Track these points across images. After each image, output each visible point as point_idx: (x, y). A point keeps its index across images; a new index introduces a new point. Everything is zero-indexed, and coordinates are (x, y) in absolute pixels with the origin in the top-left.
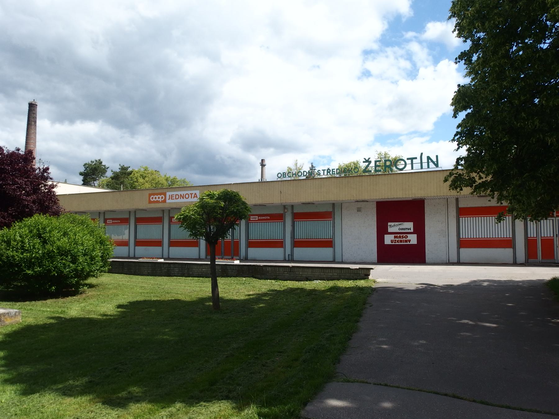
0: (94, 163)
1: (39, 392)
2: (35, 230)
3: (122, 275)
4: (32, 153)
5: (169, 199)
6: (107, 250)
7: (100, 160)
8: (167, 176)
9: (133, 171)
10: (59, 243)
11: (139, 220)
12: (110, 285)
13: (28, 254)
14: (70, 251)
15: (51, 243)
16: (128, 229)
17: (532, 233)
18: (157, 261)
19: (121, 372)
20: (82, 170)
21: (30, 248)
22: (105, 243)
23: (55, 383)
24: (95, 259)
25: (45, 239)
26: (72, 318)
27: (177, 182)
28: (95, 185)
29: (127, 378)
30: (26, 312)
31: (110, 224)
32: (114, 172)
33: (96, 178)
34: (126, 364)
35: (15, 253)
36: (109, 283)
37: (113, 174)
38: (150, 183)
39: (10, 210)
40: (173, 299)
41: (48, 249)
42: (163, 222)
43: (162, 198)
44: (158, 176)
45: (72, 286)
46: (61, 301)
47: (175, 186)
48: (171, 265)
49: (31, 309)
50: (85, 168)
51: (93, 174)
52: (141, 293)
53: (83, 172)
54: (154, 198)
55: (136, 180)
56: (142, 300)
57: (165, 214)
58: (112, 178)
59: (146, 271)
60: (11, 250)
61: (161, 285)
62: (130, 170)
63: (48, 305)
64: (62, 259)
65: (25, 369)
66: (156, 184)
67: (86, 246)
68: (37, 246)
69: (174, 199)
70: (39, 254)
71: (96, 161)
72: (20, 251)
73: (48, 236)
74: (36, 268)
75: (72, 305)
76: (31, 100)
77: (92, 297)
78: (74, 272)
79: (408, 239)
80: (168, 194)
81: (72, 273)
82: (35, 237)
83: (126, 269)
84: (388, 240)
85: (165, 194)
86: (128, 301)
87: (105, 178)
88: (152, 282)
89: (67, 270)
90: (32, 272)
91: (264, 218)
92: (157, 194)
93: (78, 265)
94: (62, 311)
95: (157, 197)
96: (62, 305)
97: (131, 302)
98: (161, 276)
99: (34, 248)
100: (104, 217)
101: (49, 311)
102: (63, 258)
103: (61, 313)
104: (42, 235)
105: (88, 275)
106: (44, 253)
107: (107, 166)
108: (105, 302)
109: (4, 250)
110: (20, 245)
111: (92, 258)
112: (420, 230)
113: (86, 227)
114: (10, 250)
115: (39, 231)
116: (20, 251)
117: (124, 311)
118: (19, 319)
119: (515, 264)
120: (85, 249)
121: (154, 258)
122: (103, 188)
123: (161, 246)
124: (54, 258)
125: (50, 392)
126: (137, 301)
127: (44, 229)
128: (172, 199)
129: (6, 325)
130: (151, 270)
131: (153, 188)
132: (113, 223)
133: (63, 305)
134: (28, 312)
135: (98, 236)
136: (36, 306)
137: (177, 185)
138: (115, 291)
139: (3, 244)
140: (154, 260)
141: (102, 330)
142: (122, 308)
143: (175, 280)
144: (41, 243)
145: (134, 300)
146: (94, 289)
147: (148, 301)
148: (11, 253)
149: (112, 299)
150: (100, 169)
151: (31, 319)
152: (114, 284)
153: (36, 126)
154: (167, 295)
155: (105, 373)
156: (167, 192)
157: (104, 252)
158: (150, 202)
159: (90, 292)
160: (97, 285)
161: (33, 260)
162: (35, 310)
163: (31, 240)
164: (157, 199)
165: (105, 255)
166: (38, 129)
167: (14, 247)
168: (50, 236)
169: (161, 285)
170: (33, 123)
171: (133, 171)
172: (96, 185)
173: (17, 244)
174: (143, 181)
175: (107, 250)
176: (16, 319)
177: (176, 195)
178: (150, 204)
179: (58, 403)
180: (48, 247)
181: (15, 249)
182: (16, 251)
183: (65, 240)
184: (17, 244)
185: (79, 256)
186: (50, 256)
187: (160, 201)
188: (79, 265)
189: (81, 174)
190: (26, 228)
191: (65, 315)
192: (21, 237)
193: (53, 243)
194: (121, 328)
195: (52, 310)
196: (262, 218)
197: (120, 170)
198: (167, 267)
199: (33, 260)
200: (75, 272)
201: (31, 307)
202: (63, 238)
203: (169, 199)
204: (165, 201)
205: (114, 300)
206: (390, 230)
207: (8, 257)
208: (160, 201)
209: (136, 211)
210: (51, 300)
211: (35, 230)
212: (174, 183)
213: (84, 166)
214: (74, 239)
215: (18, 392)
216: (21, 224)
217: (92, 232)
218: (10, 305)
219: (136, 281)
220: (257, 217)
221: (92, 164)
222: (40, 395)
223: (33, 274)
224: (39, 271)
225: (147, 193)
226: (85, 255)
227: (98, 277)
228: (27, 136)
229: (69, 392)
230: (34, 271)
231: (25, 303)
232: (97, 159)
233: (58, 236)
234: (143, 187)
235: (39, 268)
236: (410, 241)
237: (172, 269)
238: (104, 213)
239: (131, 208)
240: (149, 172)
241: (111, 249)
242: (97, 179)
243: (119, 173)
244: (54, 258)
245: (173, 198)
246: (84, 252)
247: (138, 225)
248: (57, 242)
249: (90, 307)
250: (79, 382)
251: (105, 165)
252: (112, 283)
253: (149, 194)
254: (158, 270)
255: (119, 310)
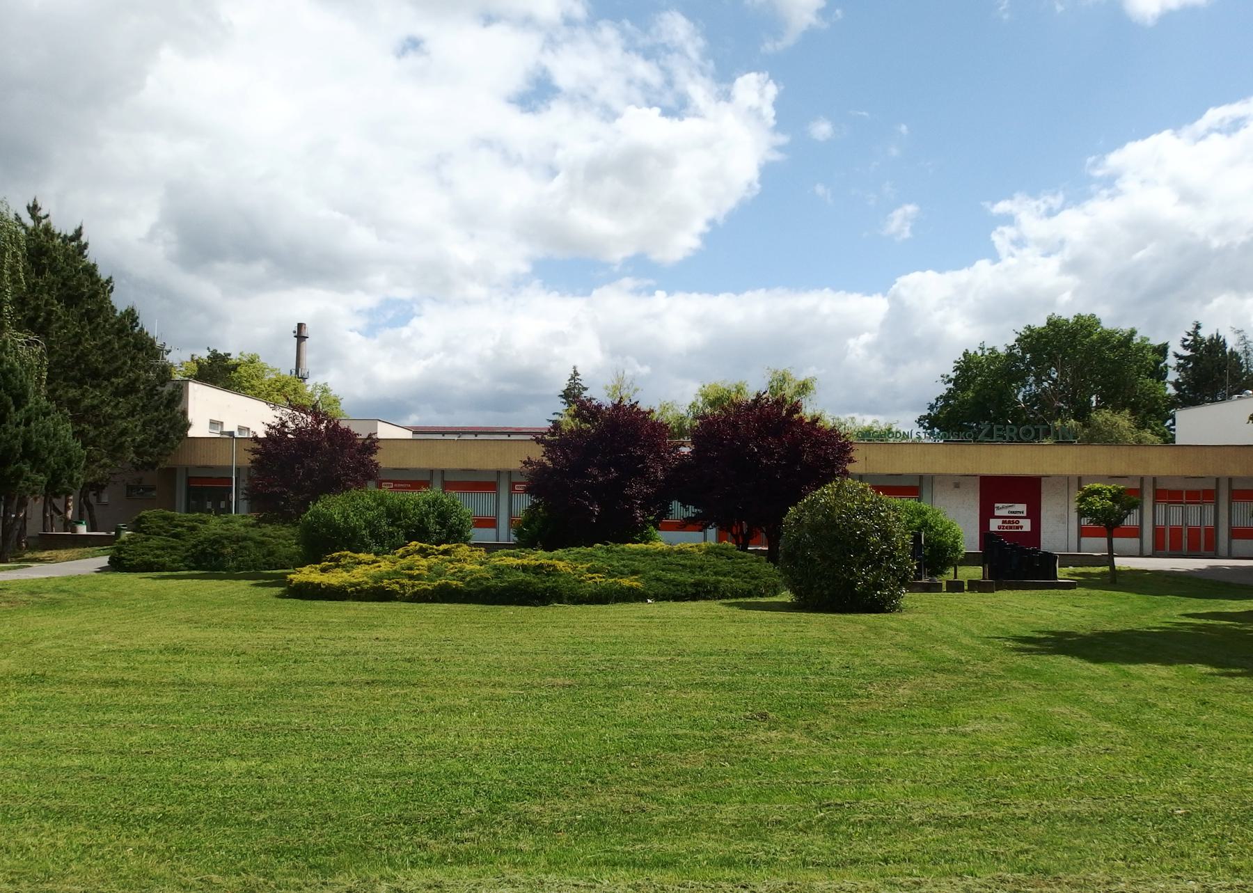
17: (1161, 522)
42: (1172, 553)
79: (1019, 525)
84: (994, 525)
100: (1141, 543)
112: (1034, 515)
119: (1141, 555)
196: (400, 485)
206: (997, 513)
236: (1022, 527)
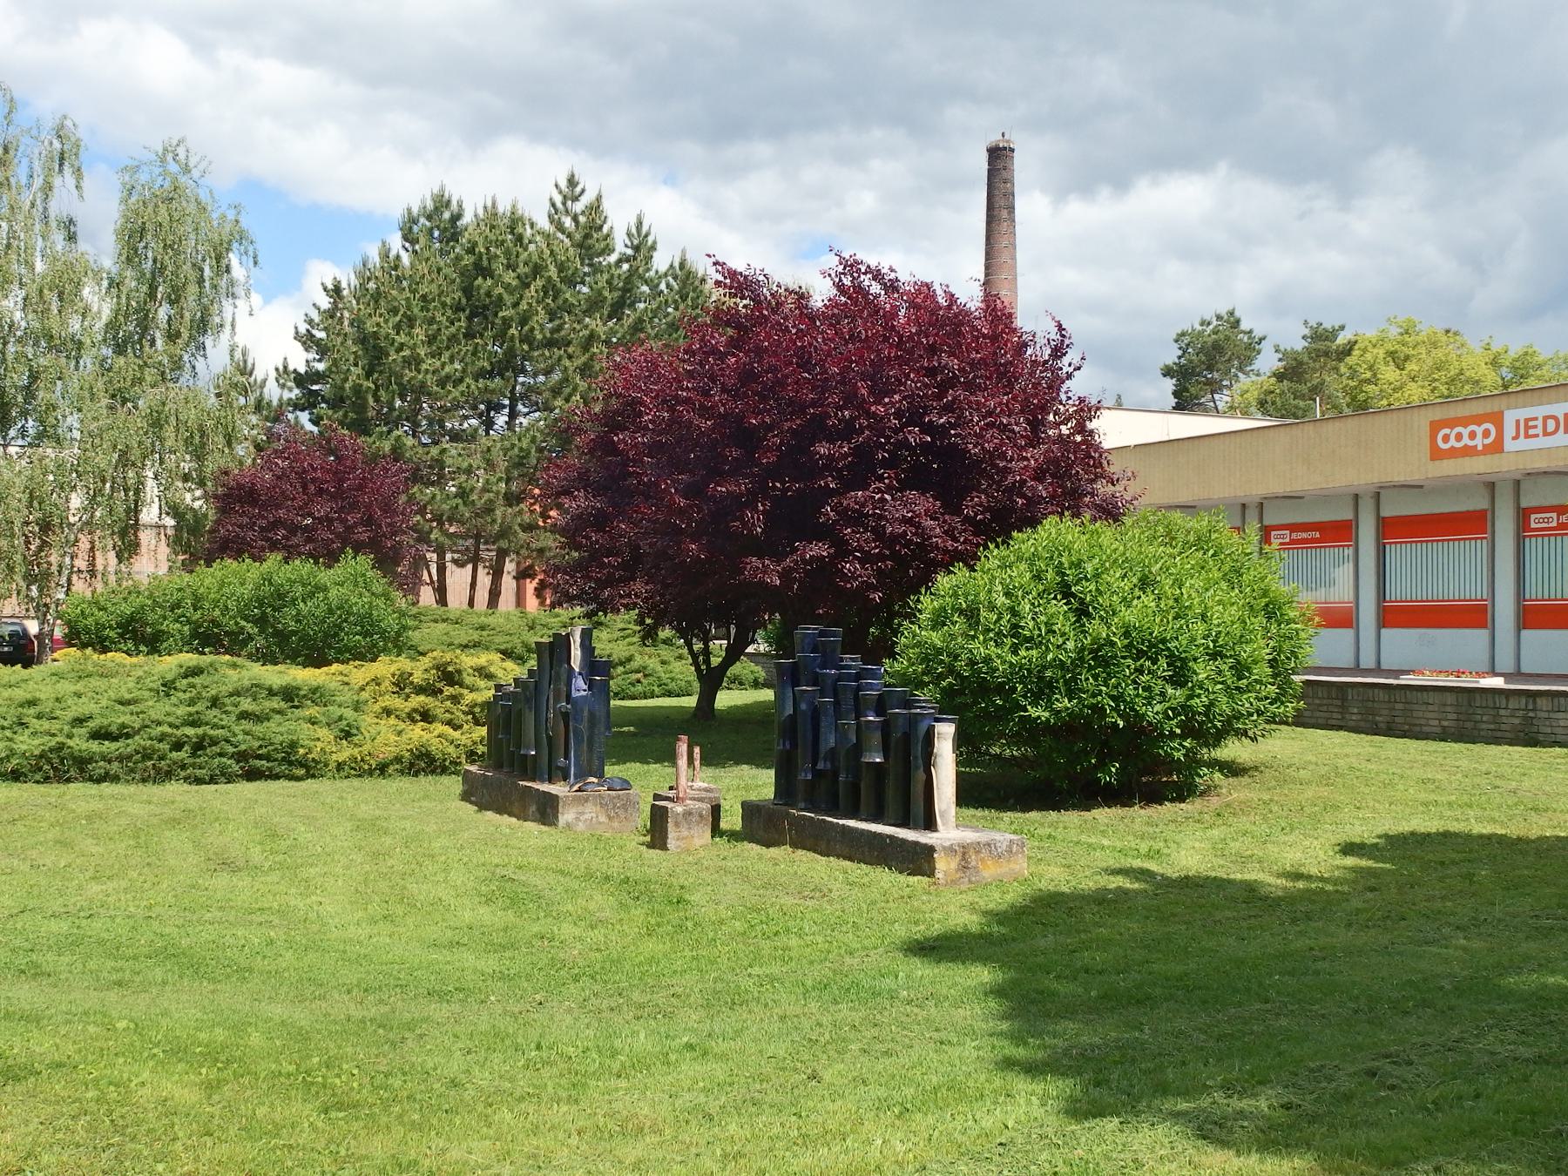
0: (1211, 327)
1: (1118, 1115)
2: (1050, 570)
3: (1342, 733)
4: (1010, 315)
5: (1516, 438)
6: (1292, 639)
7: (1231, 313)
8: (1496, 348)
9: (1356, 342)
10: (1129, 616)
11: (1391, 529)
12: (1304, 769)
13: (1034, 652)
14: (1164, 641)
15: (1102, 613)
16: (1351, 565)
18: (1477, 682)
19: (1392, 1087)
20: (1171, 356)
21: (1037, 632)
22: (1282, 615)
23: (1164, 1090)
24: (1249, 669)
25: (1082, 601)
26: (1187, 877)
27: (1540, 367)
28: (1216, 408)
29: (1420, 1116)
30: (1037, 843)
31: (1545, 533)
32: (1285, 353)
33: (1221, 381)
34: (1410, 1063)
35: (993, 650)
36: (1297, 760)
37: (1280, 360)
38: (1427, 383)
39: (967, 507)
40: (1562, 834)
41: (1094, 634)
43: (1486, 434)
44: (1459, 353)
45: (1171, 765)
46: (1139, 815)
47: (1532, 383)
48: (1538, 700)
49: (1049, 836)
50: (1180, 348)
51: (1210, 368)
52: (1426, 804)
53: (1175, 364)
54: (1450, 439)
55: (1368, 375)
56: (1434, 831)
57: (1248, 520)
58: (1280, 376)
59: (1431, 722)
60: (981, 638)
61: (1502, 777)
62: (1342, 339)
63: (1102, 828)
64: (1140, 671)
65: (1072, 1032)
66: (1451, 381)
67: (1219, 625)
68: (1059, 626)
69: (1537, 436)
70: (1065, 650)
71: (1219, 318)
72: (1008, 641)
73: (1090, 591)
74: (1057, 700)
75: (1180, 832)
76: (994, 138)
77: (1244, 808)
78: (1181, 715)
80: (1511, 417)
81: (1173, 719)
82: (1052, 596)
83: (1355, 711)
85: (1497, 419)
86: (1380, 831)
87: (1254, 378)
88: (1464, 763)
89: (1158, 708)
90: (1047, 714)
91: (1305, 535)
92: (1465, 421)
93: (1192, 689)
94: (1150, 850)
95: (1465, 432)
96: (1145, 828)
97: (1391, 834)
98: (1497, 741)
99: (1050, 631)
101: (1108, 848)
102: (1142, 666)
103: (1148, 856)
104: (1073, 589)
105: (1229, 728)
106: (1083, 649)
107: (1258, 333)
108: (1292, 829)
109: (960, 639)
110: (1008, 621)
111: (1240, 669)
113: (1213, 556)
114: (978, 638)
115: (1064, 574)
116: (1008, 641)
117: (1370, 872)
118: (1021, 866)
120: (1214, 634)
121: (1463, 673)
122: (1246, 414)
123: (1485, 626)
124: (1114, 664)
125: (1155, 1119)
126: (1413, 834)
127: (1077, 565)
128: (1527, 436)
129: (984, 882)
130: (1454, 716)
131: (1439, 400)
132: (1292, 542)
133: (1151, 830)
134: (1042, 844)
135: (1255, 587)
136: (1065, 828)
137: (1539, 378)
138: (1324, 792)
139: (955, 618)
140: (1466, 682)
141: (1298, 929)
142: (1361, 856)
143: (1558, 760)
144: (1071, 615)
145: (1401, 829)
146: (1245, 780)
147: (1456, 835)
148: (982, 649)
149: (1316, 820)
150: (1235, 346)
151: (1057, 870)
152: (1316, 764)
153: (1014, 221)
154: (1534, 817)
155: (1334, 1084)
156: (1508, 409)
157: (1280, 646)
158: (1437, 454)
159: (1232, 791)
160: (1256, 768)
161: (1048, 674)
162: (1063, 841)
163: (1039, 605)
164: (1466, 441)
165: (1283, 657)
166: (1019, 230)
167: (989, 630)
168: (1097, 590)
169: (1502, 777)
170: (1004, 214)
171: (1356, 342)
172: (1221, 405)
173: (999, 619)
174: (1398, 378)
175: (1292, 639)
176: (1012, 866)
177: (1546, 418)
178: (1437, 462)
179: (1183, 1160)
180: (1096, 628)
181: (991, 635)
182: (996, 641)
183: (1146, 603)
184: (999, 619)
185: (1195, 660)
186: (1100, 658)
187: (1480, 448)
188: (1198, 691)
189: (1168, 372)
190: (1023, 566)
191: (1164, 865)
192: (1007, 594)
193: (1107, 612)
194: (1367, 927)
195: (1119, 845)
197: (1307, 344)
198: (1523, 707)
199: (1048, 674)
200: (1121, 724)
201: (1048, 831)
202: (1139, 598)
203: (1516, 438)
204: (1497, 447)
205: (1325, 823)
207: (972, 663)
208: (1476, 446)
209: (1382, 491)
210: (1106, 809)
211: (1050, 570)
212: (1521, 372)
213: (1176, 341)
214: (1176, 600)
215: (1050, 1102)
216: (1007, 553)
217: (1234, 576)
218: (984, 818)
219: (1400, 759)
220: (1554, 515)
221: (1204, 331)
222: (1121, 1123)
223: (1048, 720)
224: (1068, 709)
225: (1422, 420)
226: (1215, 655)
227: (1259, 738)
228: (986, 260)
229: (1217, 1130)
230: (1053, 709)
231: (1027, 815)
232: (1223, 312)
233: (1124, 592)
234: (1399, 400)
235: (1066, 700)
237: (1545, 715)
238: (1377, 497)
239: (1362, 482)
240: (1419, 338)
241: (1303, 635)
242: (1225, 383)
243: (1306, 355)
244: (1114, 664)
245: (1531, 432)
246: (1211, 645)
247: (1388, 547)
248: (1120, 611)
249: (1243, 842)
250: (1244, 1101)
251: (1250, 332)
252: (1310, 762)
253: (1431, 422)
254: (1485, 719)
255: (1350, 861)
